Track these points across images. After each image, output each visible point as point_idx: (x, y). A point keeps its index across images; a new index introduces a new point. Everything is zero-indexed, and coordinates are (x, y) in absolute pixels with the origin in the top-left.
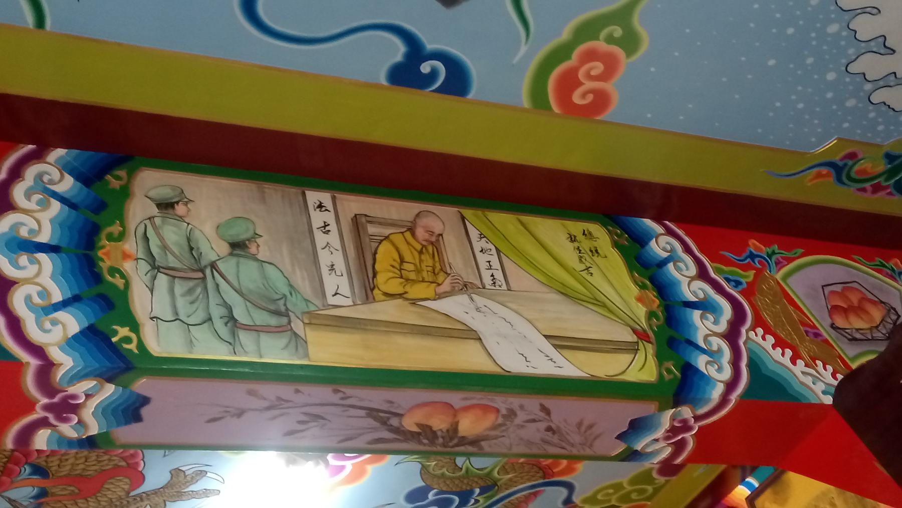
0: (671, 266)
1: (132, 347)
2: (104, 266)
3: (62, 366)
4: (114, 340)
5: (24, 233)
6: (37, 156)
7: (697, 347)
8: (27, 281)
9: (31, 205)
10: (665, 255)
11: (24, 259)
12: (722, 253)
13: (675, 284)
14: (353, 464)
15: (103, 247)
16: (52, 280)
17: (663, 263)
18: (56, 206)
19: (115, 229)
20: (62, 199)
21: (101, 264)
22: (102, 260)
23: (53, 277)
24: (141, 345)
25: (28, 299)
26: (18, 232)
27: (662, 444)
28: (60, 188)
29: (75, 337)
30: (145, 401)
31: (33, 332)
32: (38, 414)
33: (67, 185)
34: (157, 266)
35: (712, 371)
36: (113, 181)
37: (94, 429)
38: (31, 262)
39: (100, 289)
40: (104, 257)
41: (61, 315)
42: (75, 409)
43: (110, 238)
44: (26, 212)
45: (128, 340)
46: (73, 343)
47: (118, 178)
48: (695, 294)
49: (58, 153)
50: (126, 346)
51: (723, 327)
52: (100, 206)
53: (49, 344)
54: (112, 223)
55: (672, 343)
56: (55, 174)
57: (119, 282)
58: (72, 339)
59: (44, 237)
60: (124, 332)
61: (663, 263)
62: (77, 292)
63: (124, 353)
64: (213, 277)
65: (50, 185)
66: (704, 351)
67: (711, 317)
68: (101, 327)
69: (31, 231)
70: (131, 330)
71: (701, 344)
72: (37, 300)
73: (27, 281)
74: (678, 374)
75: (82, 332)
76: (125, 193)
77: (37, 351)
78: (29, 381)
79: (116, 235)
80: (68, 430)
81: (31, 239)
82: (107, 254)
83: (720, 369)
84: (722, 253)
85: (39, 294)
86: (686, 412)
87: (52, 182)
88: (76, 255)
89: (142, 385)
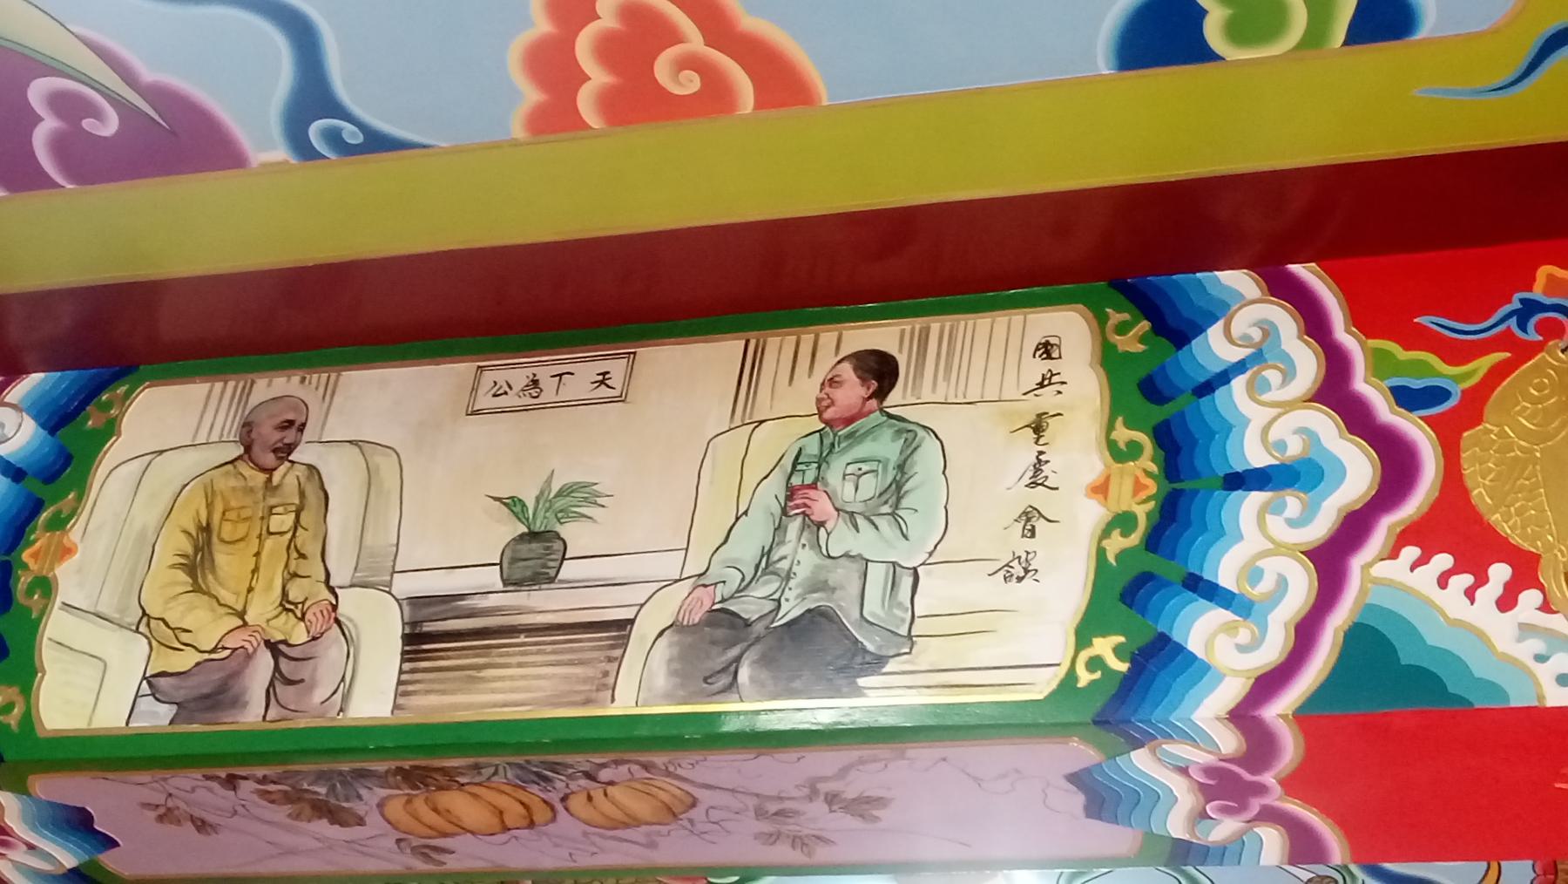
1: (1115, 317)
2: (1148, 462)
3: (1468, 602)
4: (1145, 325)
5: (1293, 503)
8: (1287, 406)
9: (1273, 567)
16: (1289, 796)
18: (1226, 573)
19: (1116, 544)
21: (1154, 468)
22: (1148, 473)
24: (1101, 319)
25: (1288, 374)
26: (1305, 505)
29: (1215, 320)
34: (1141, 347)
38: (1246, 337)
39: (1160, 413)
41: (1233, 355)
42: (1207, 793)
45: (1122, 329)
47: (1095, 663)
50: (1126, 316)
54: (1122, 555)
57: (1122, 434)
58: (1219, 315)
59: (1254, 499)
62: (1204, 401)
64: (784, 616)
69: (1279, 509)
72: (1273, 376)
73: (1287, 406)
75: (1200, 330)
79: (1116, 534)
81: (1276, 493)
82: (1138, 487)
85: (1267, 386)
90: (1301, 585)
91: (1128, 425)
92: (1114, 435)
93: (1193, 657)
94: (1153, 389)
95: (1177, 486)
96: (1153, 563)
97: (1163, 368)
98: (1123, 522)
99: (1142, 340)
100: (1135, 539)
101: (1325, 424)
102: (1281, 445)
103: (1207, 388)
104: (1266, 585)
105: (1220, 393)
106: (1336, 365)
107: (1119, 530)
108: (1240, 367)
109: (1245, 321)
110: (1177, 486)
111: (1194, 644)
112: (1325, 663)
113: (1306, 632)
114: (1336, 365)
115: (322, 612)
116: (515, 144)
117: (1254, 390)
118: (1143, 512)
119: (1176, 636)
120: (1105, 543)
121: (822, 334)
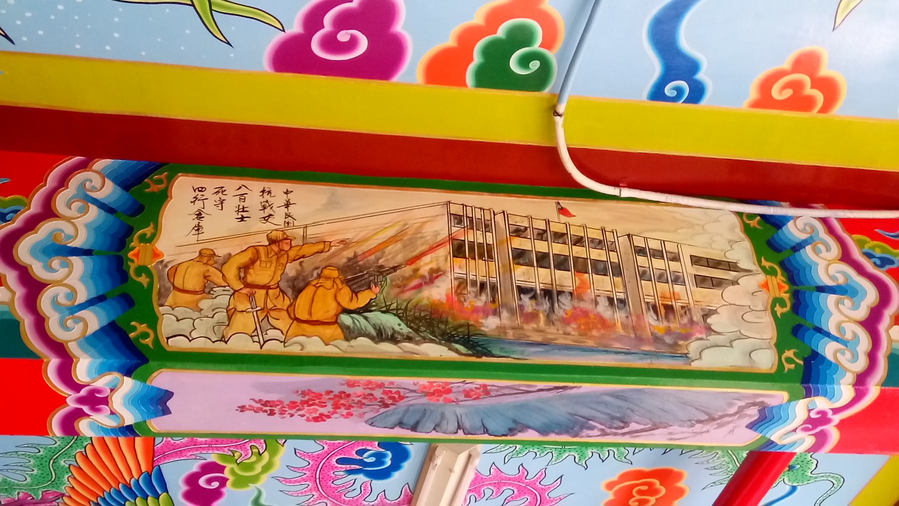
0: (808, 248)
1: (148, 341)
4: (132, 335)
6: (82, 166)
7: (828, 335)
8: (59, 283)
10: (803, 236)
11: (56, 262)
12: (876, 230)
13: (809, 267)
14: (223, 473)
15: (133, 248)
17: (798, 247)
18: (94, 212)
19: (148, 231)
20: (102, 206)
23: (82, 279)
27: (800, 434)
28: (98, 195)
29: (95, 334)
30: (169, 395)
31: (54, 329)
32: (71, 404)
33: (108, 191)
35: (844, 359)
36: (152, 186)
37: (130, 419)
39: (781, 256)
40: (783, 284)
41: (85, 314)
42: (106, 401)
43: (143, 239)
44: (68, 219)
45: (145, 335)
46: (92, 341)
47: (789, 360)
48: (833, 278)
49: (102, 164)
51: (862, 313)
52: (137, 209)
53: (67, 342)
55: (797, 331)
56: (97, 181)
57: (143, 280)
60: (142, 328)
61: (798, 247)
63: (140, 348)
65: (92, 192)
66: (836, 339)
67: (847, 302)
68: (120, 324)
70: (149, 327)
71: (833, 331)
72: (62, 300)
73: (59, 283)
74: (801, 362)
75: (103, 330)
76: (164, 196)
77: (59, 348)
78: (51, 375)
79: (149, 235)
80: (103, 419)
82: (780, 287)
83: (855, 358)
84: (876, 230)
86: (821, 403)
87: (94, 189)
88: (802, 284)
89: (163, 379)
90: (60, 202)
91: (141, 284)
92: (147, 280)
93: (830, 363)
94: (127, 301)
95: (117, 253)
96: (131, 221)
97: (124, 311)
98: (777, 301)
99: (134, 329)
100: (787, 309)
101: (39, 271)
102: (63, 265)
103: (100, 299)
104: (76, 205)
105: (93, 295)
106: (31, 303)
107: (146, 237)
108: (82, 307)
109: (77, 330)
110: (117, 253)
111: (110, 185)
112: (884, 369)
113: (872, 356)
114: (31, 303)
115: (520, 256)
116: (418, 85)
117: (73, 292)
118: (134, 243)
119: (119, 189)
120: (153, 231)
121: (156, 438)
